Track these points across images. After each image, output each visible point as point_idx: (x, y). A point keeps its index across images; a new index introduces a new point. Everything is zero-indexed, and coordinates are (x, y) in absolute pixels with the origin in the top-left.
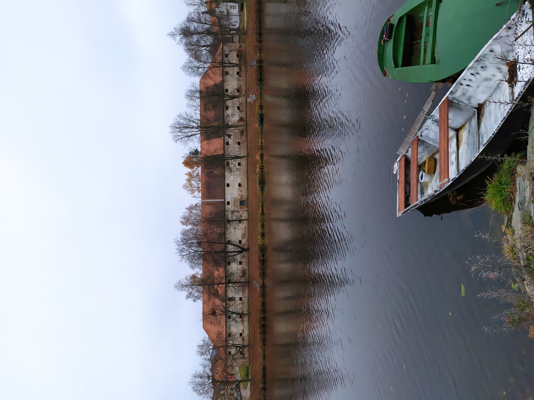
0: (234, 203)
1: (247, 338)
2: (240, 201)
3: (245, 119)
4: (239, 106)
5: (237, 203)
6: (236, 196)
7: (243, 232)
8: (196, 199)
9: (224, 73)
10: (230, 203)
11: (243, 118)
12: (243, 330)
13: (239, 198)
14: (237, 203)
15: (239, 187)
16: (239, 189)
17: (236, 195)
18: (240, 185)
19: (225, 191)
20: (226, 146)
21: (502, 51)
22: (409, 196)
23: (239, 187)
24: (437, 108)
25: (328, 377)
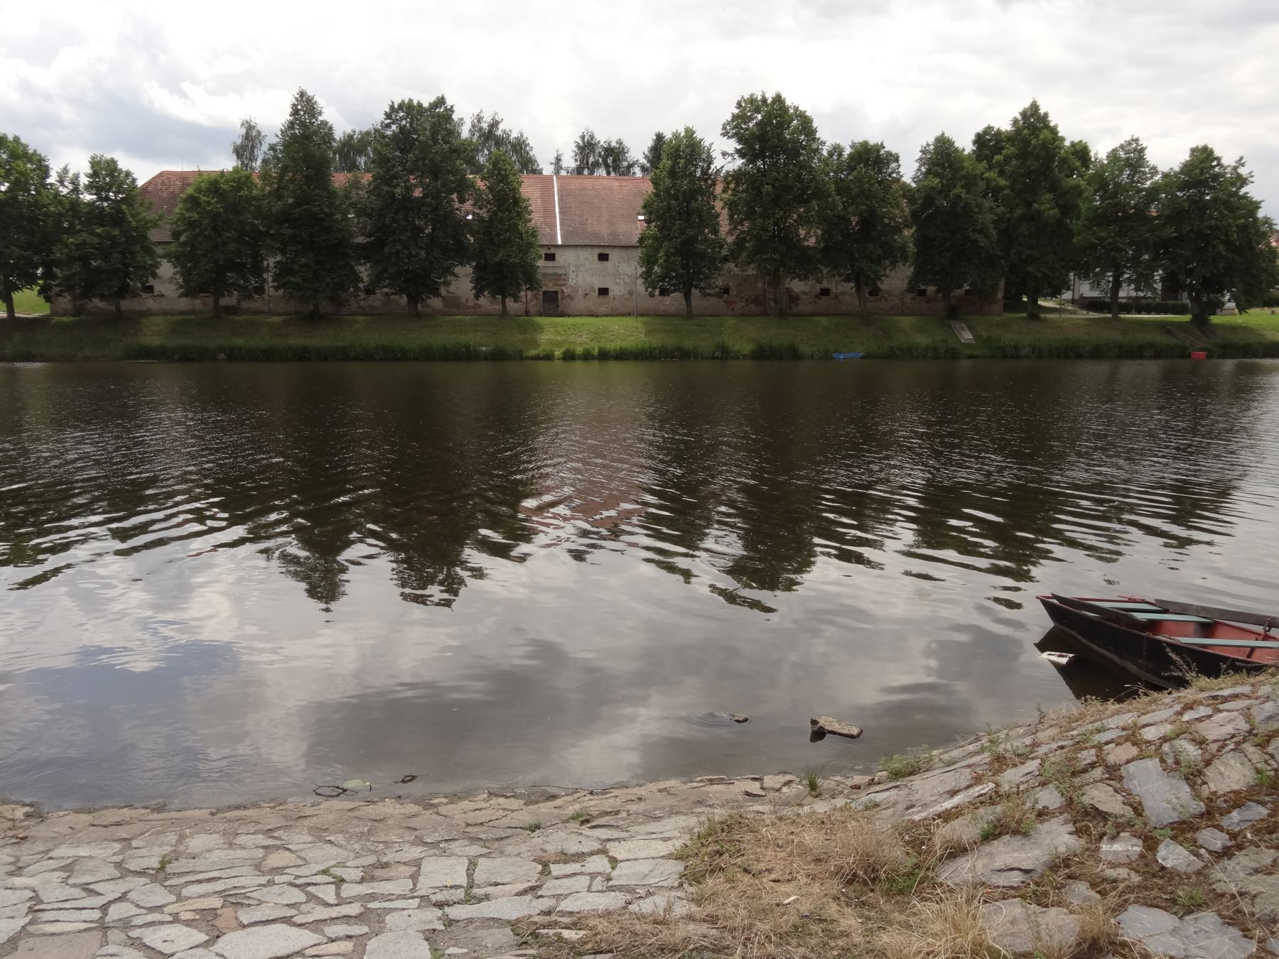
0: (551, 275)
1: (137, 308)
2: (557, 292)
3: (795, 310)
4: (831, 294)
5: (551, 284)
6: (572, 281)
7: (463, 301)
8: (1177, 169)
9: (605, 251)
10: (550, 264)
11: (797, 305)
12: (162, 296)
13: (565, 290)
14: (551, 284)
15: (599, 289)
16: (592, 289)
17: (574, 281)
18: (603, 292)
19: (585, 249)
20: (597, 251)
21: (251, 902)
22: (1214, 590)
23: (599, 289)
24: (1211, 651)
25: (179, 498)
